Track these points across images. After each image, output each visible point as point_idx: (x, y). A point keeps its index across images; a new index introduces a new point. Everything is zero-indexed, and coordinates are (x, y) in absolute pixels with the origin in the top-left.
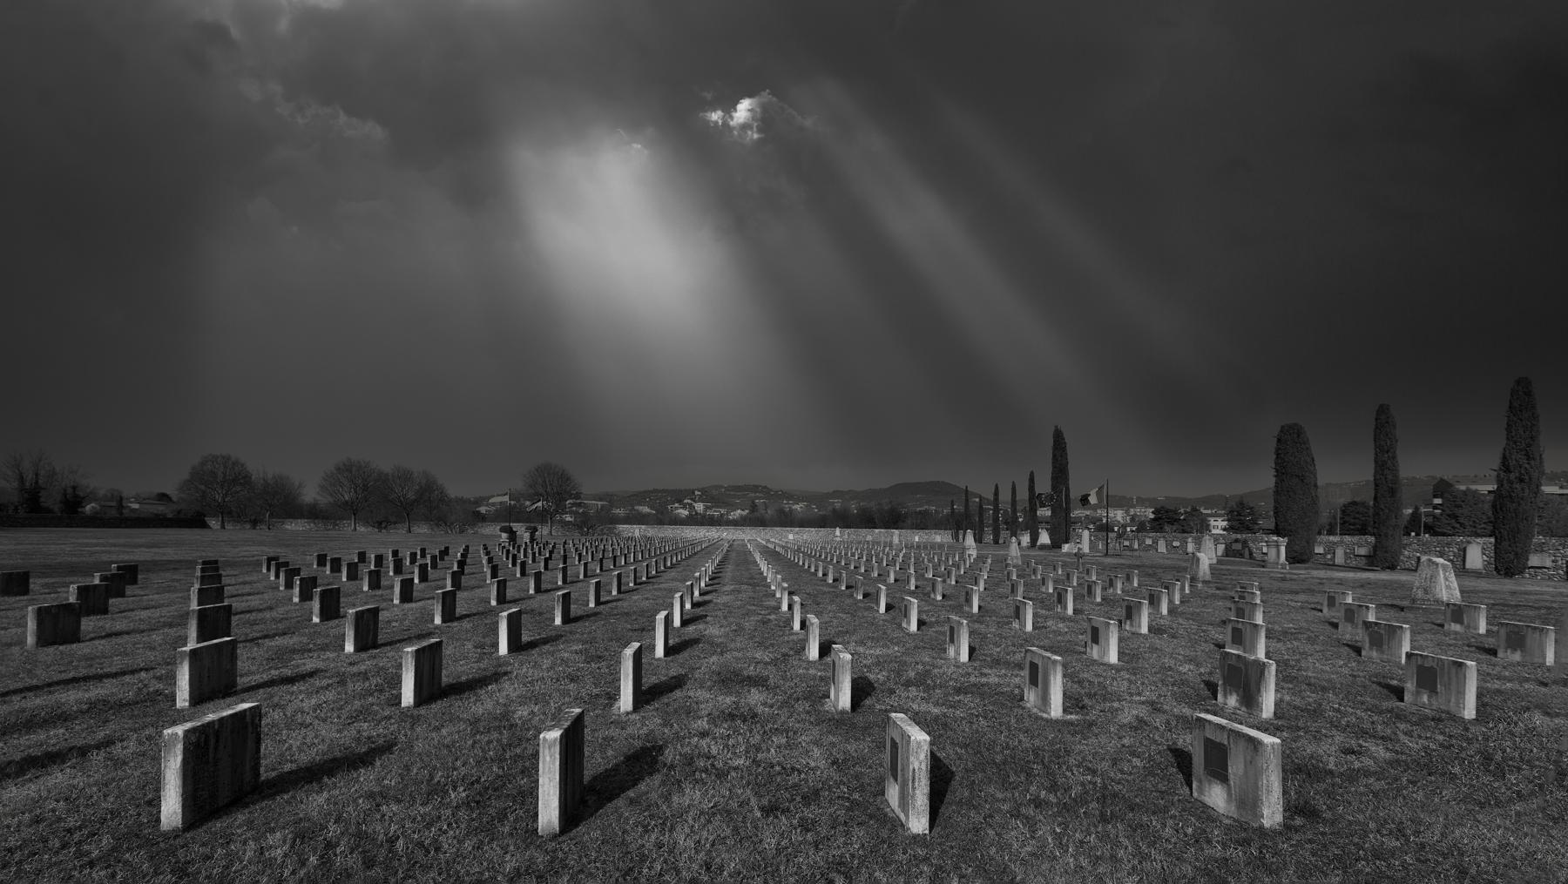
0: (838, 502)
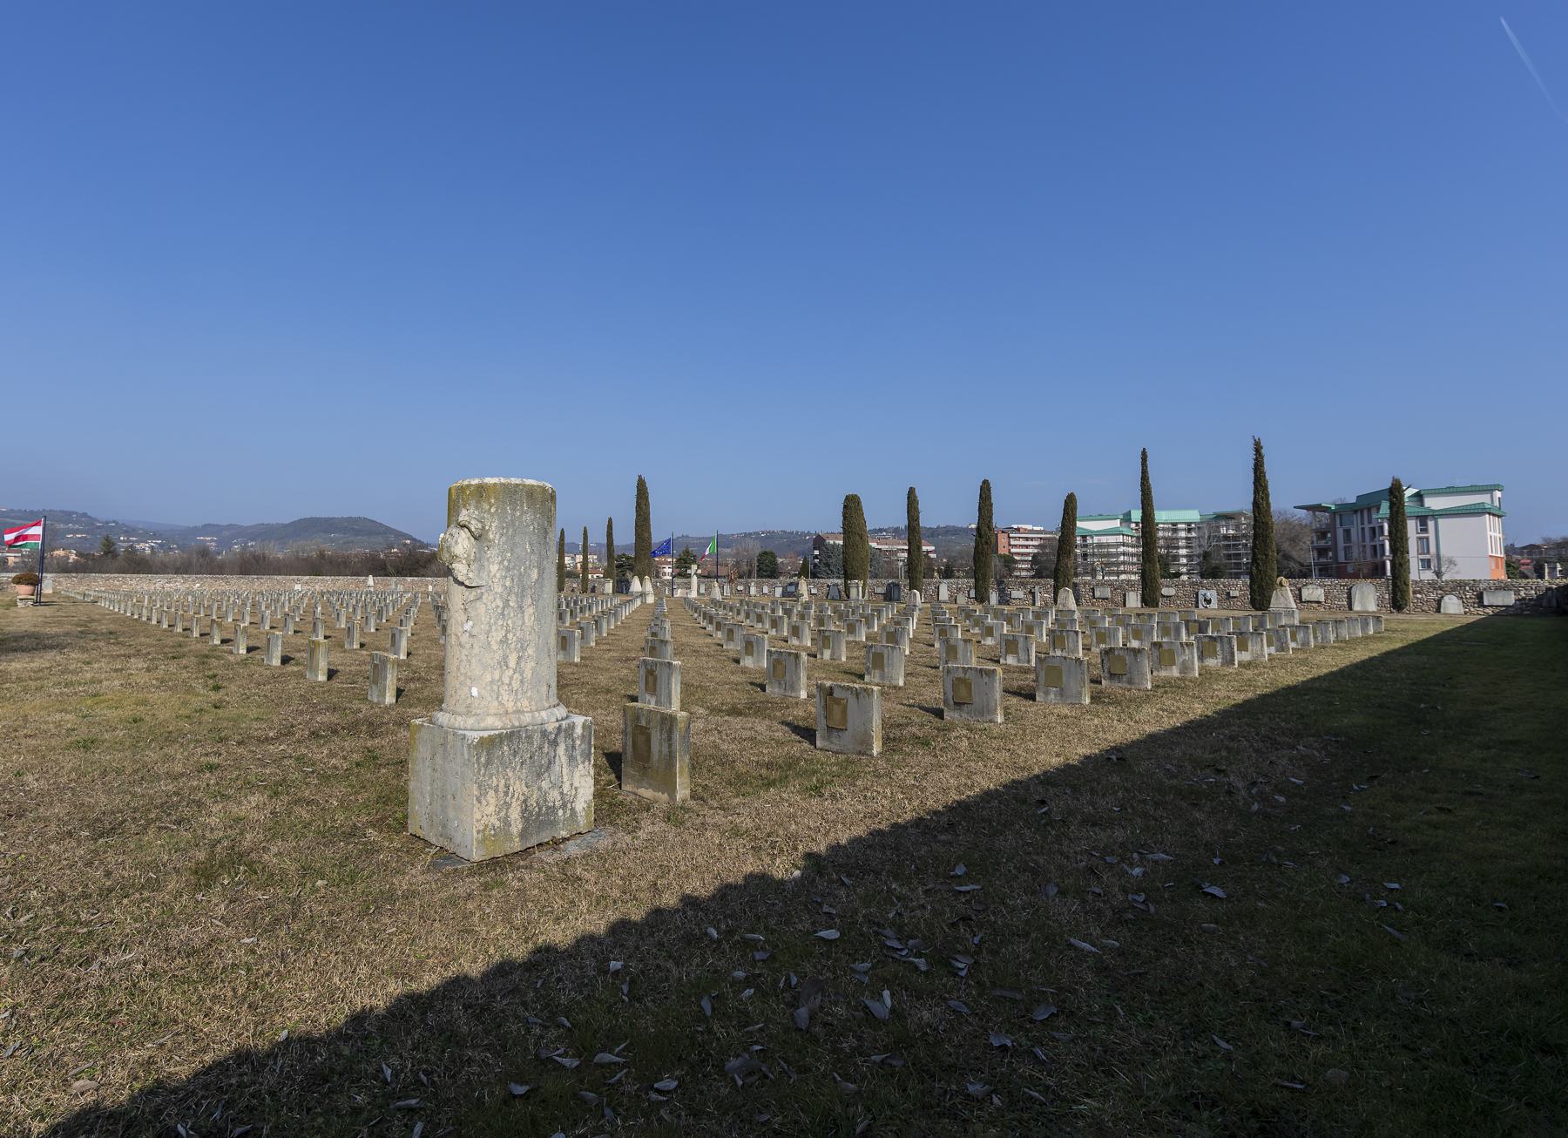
0: (212, 541)
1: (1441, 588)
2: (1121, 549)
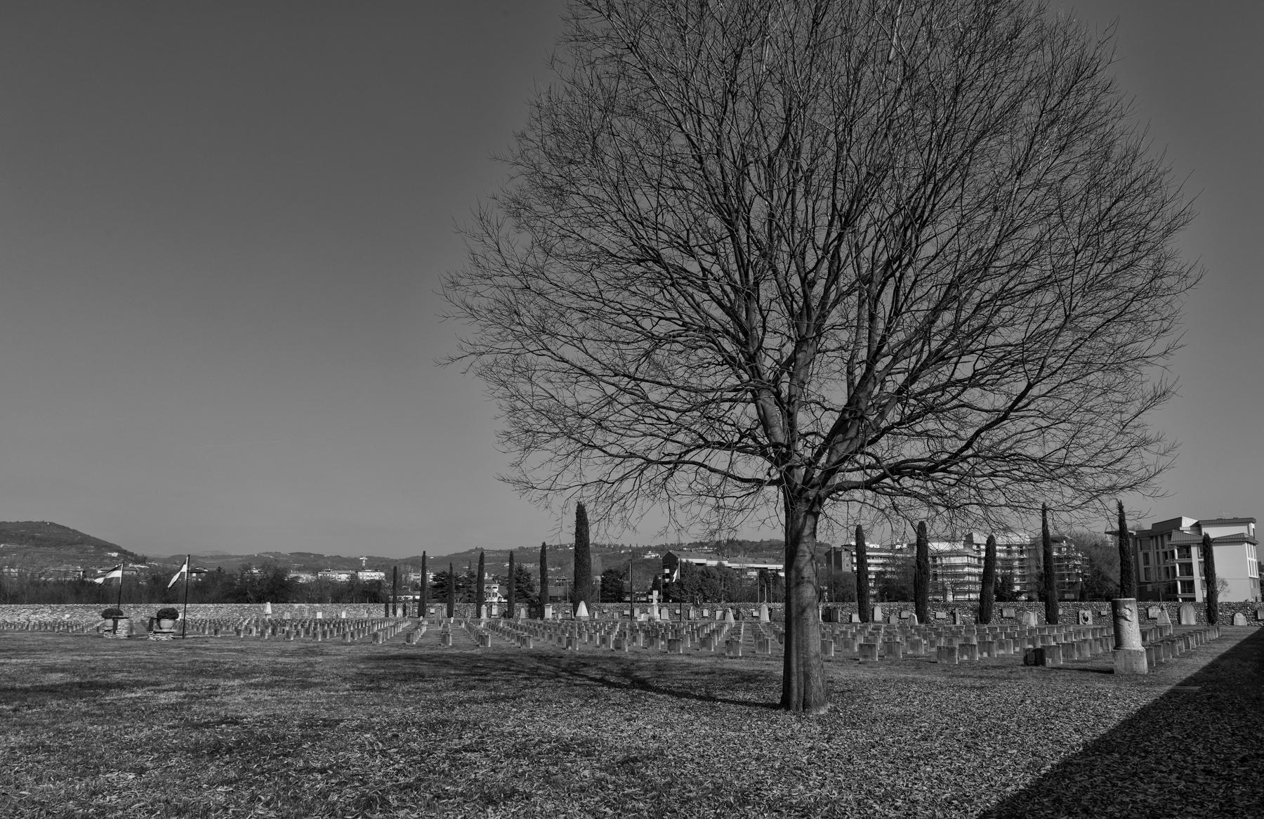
1: (1233, 608)
2: (966, 570)
